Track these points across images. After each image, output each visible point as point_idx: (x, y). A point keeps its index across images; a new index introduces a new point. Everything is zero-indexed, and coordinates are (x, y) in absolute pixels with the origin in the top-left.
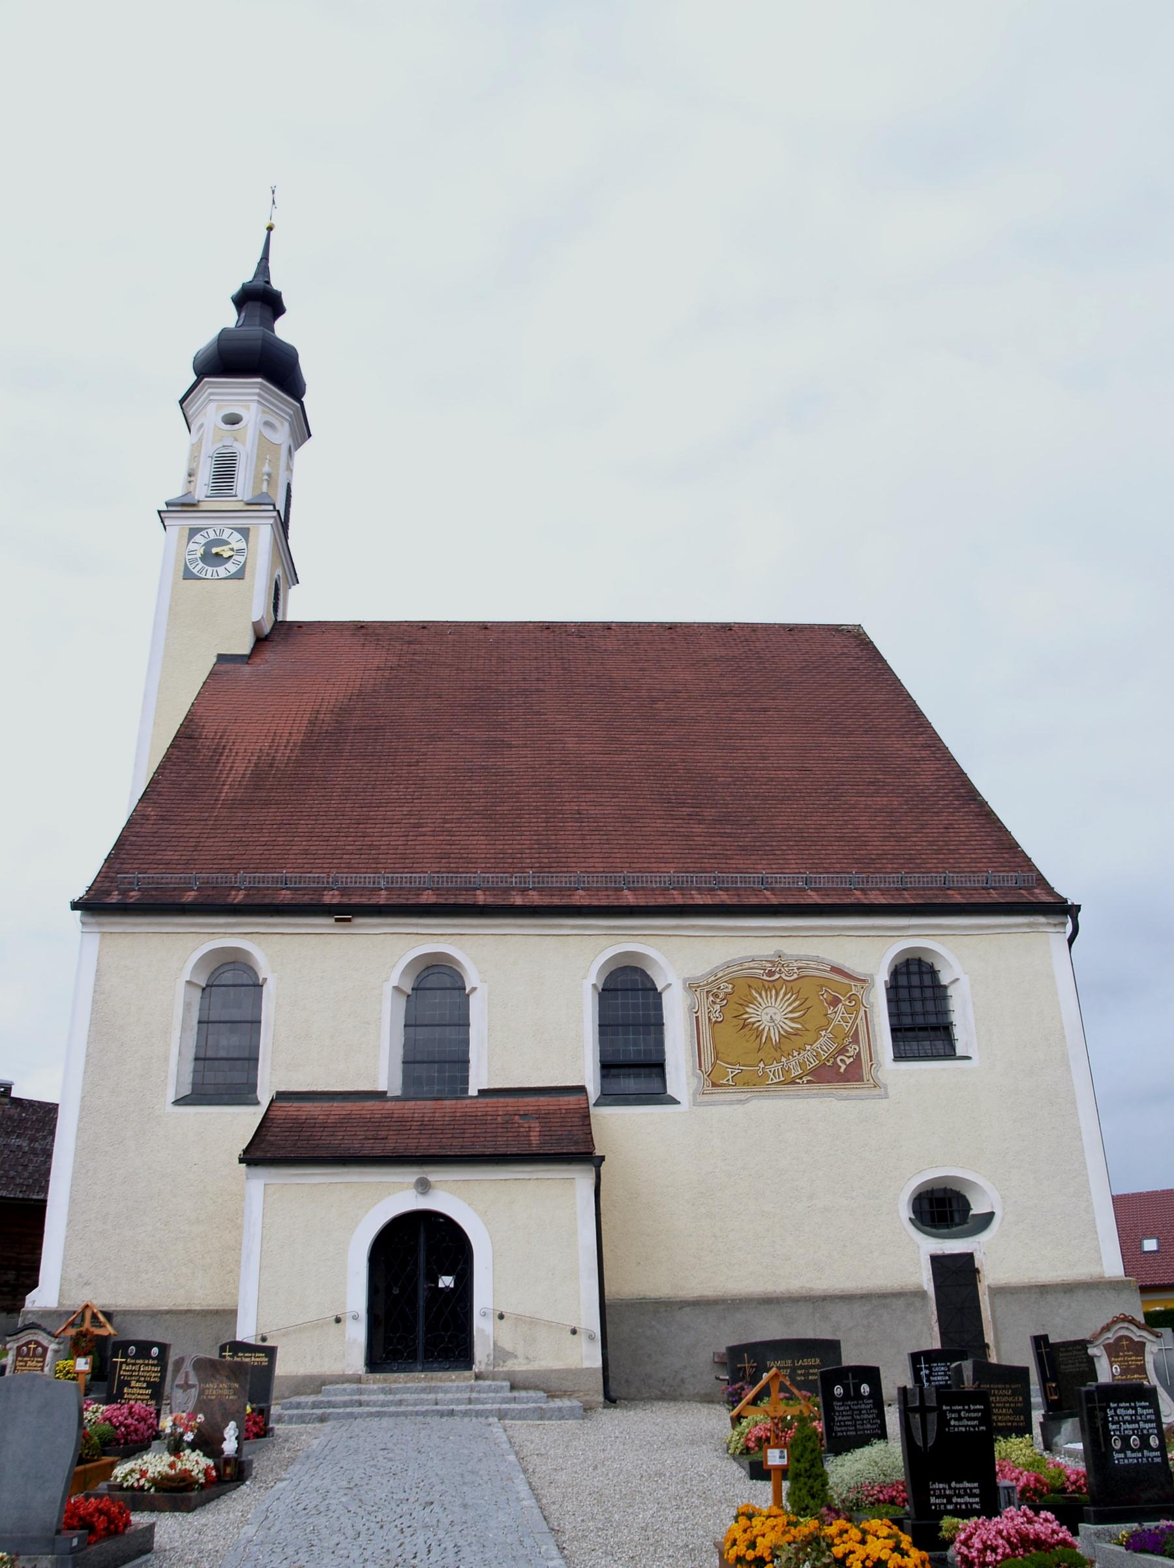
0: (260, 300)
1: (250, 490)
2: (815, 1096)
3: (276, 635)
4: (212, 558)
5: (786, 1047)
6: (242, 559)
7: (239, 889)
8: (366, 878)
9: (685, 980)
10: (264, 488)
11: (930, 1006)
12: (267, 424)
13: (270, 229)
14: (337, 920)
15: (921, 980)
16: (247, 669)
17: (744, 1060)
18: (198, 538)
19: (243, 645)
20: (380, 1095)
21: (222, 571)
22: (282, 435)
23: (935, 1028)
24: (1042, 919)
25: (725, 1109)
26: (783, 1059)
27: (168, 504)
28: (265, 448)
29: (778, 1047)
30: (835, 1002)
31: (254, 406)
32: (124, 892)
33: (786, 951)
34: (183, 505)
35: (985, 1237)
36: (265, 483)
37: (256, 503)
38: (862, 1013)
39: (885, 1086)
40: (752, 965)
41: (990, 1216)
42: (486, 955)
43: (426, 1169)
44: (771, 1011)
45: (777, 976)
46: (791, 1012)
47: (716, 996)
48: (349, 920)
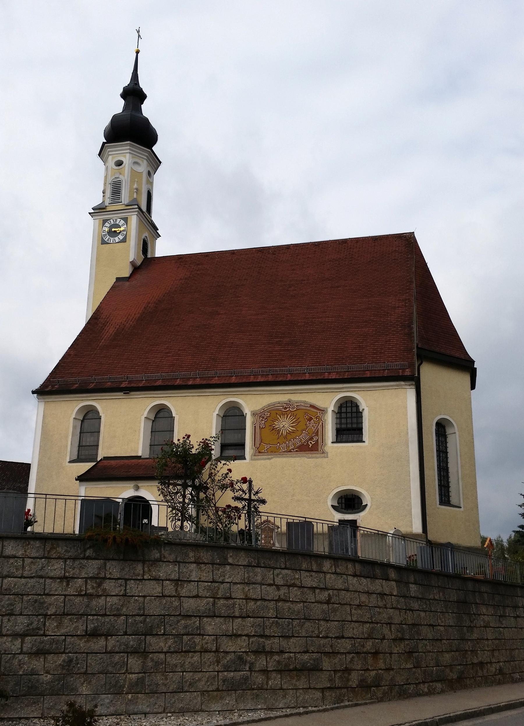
0: (134, 94)
2: (299, 457)
3: (147, 263)
4: (112, 234)
5: (289, 437)
6: (125, 233)
7: (93, 383)
8: (138, 376)
9: (252, 412)
10: (135, 196)
11: (355, 420)
12: (135, 163)
13: (138, 52)
16: (127, 284)
17: (273, 442)
18: (107, 224)
19: (126, 272)
20: (139, 457)
22: (143, 168)
23: (354, 429)
24: (402, 383)
25: (263, 461)
27: (93, 209)
28: (134, 174)
29: (285, 437)
30: (311, 419)
32: (53, 386)
34: (100, 209)
35: (362, 514)
36: (135, 194)
37: (134, 204)
39: (327, 453)
40: (278, 405)
41: (367, 505)
43: (137, 482)
48: (128, 393)
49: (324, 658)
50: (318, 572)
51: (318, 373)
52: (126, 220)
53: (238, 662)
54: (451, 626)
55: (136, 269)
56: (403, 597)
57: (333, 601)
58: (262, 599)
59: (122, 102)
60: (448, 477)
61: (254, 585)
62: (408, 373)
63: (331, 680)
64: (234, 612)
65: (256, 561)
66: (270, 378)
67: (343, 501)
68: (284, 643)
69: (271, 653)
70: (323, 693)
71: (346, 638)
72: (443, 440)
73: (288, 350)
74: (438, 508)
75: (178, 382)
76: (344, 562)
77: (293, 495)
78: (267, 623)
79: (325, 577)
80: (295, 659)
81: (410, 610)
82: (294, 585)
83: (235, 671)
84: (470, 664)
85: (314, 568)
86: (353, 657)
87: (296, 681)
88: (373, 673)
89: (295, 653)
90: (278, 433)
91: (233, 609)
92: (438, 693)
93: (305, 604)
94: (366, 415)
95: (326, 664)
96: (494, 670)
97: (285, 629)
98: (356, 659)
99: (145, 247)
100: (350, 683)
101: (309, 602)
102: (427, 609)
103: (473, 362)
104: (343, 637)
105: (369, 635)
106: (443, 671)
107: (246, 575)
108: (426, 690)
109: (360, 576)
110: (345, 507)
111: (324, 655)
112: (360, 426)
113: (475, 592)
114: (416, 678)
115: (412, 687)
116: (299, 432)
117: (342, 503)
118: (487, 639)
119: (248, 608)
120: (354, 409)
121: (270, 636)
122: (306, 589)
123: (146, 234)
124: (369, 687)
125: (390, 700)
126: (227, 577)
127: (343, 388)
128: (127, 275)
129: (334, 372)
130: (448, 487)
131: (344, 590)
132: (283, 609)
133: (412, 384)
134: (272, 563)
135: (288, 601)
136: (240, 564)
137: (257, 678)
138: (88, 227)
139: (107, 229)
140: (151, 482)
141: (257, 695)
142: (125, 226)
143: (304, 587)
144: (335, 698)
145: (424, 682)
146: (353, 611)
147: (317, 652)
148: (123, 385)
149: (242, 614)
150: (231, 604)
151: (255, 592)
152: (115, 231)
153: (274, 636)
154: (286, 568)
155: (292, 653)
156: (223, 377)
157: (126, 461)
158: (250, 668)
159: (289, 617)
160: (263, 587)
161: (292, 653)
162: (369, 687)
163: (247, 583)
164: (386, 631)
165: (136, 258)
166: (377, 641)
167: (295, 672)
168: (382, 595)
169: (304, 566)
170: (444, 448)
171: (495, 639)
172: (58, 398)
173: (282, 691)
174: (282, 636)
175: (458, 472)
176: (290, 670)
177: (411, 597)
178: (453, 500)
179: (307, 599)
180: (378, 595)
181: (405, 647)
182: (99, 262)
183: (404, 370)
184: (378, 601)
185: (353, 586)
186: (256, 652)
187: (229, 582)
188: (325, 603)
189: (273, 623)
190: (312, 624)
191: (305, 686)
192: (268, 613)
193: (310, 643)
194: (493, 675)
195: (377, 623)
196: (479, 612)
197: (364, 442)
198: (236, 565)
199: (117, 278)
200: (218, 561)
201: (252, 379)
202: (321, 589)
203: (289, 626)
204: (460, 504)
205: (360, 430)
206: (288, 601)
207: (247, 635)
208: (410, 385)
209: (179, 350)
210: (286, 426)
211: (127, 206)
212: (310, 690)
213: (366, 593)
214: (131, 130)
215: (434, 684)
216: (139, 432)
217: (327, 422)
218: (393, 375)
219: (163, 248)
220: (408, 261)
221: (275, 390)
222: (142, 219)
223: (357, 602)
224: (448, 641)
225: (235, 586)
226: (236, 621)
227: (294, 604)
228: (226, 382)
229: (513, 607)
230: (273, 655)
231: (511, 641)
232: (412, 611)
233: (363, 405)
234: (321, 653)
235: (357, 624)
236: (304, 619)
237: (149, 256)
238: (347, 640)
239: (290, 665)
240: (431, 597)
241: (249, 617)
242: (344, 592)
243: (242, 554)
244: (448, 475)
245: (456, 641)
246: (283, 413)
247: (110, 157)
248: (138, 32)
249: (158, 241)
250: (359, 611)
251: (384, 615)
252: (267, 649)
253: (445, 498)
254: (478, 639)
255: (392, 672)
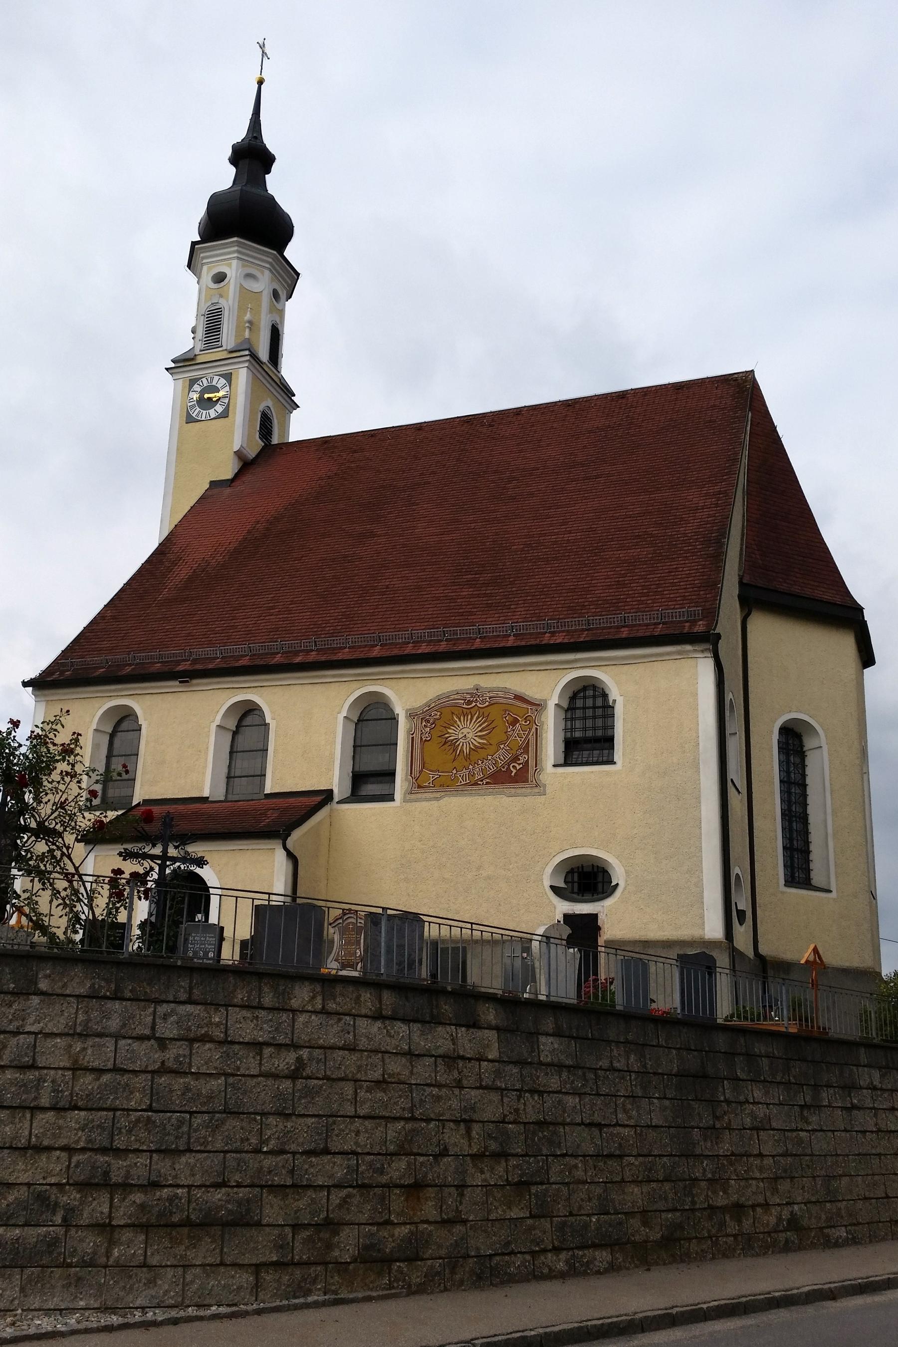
0: (252, 157)
1: (233, 338)
3: (267, 451)
4: (206, 403)
5: (474, 757)
6: (226, 401)
7: (130, 665)
8: (209, 651)
9: (407, 711)
10: (247, 334)
12: (249, 276)
13: (261, 82)
14: (180, 682)
15: (585, 703)
16: (228, 491)
18: (197, 388)
21: (212, 413)
22: (263, 284)
23: (597, 740)
24: (688, 647)
25: (424, 804)
26: (471, 767)
28: (246, 297)
29: (468, 758)
30: (515, 721)
31: (235, 263)
33: (482, 685)
35: (608, 902)
38: (534, 730)
40: (456, 697)
41: (617, 884)
42: (275, 698)
44: (465, 731)
45: (474, 704)
46: (480, 731)
47: (428, 721)
49: (268, 1197)
50: (277, 1009)
51: (531, 634)
52: (228, 377)
53: (35, 1207)
54: (656, 1126)
55: (246, 465)
56: (515, 1063)
57: (308, 1071)
58: (116, 1070)
59: (233, 170)
60: (807, 833)
61: (97, 1040)
62: (700, 627)
63: (281, 1247)
64: (36, 1098)
65: (113, 986)
66: (443, 647)
67: (576, 879)
68: (163, 1166)
69: (126, 1187)
70: (257, 1274)
71: (335, 1153)
72: (798, 760)
73: (485, 595)
74: (783, 893)
75: (278, 659)
76: (351, 989)
77: (478, 868)
78: (123, 1122)
79: (294, 1020)
80: (189, 1202)
81: (532, 1092)
82: (205, 1039)
83: (26, 1224)
84: (705, 1209)
85: (268, 999)
86: (349, 1196)
87: (187, 1248)
88: (405, 1230)
89: (189, 1187)
90: (455, 750)
91: (37, 1089)
92: (598, 1273)
93: (231, 1080)
94: (619, 711)
95: (273, 1210)
96: (773, 1220)
97: (169, 1134)
98: (356, 1200)
99: (266, 426)
100: (336, 1253)
101: (244, 1076)
102: (588, 1090)
103: (860, 610)
104: (326, 1151)
105: (401, 1147)
106: (620, 1223)
107: (81, 1017)
108: (561, 1266)
109: (393, 1018)
110: (579, 889)
111: (269, 1193)
112: (609, 733)
113: (734, 1054)
114: (532, 1241)
115: (518, 1260)
116: (494, 748)
117: (573, 882)
118: (761, 1155)
119: (76, 1089)
120: (599, 702)
121: (127, 1151)
122: (237, 1047)
123: (269, 403)
124: (388, 1261)
125: (446, 1290)
126: (31, 1020)
127: (576, 661)
128: (229, 475)
129: (563, 632)
130: (808, 852)
131: (340, 1048)
132: (171, 1091)
133: (706, 650)
134: (154, 991)
135: (185, 1073)
136: (68, 992)
137: (81, 1240)
138: (162, 396)
139: (195, 396)
140: (214, 843)
141: (79, 1279)
142: (227, 388)
143: (232, 1043)
144: (288, 1286)
145: (556, 1250)
146: (362, 1094)
147: (251, 1186)
148: (180, 668)
149: (57, 1103)
150: (31, 1081)
151: (98, 1054)
152: (210, 399)
153: (137, 1151)
154: (190, 1001)
155: (183, 1186)
156: (360, 647)
157: (180, 807)
158: (65, 1219)
159: (183, 1109)
160: (122, 1043)
161: (183, 1186)
162: (388, 1261)
163: (80, 1035)
164: (454, 1137)
165: (245, 446)
166: (421, 1159)
167: (185, 1230)
168: (451, 1059)
169: (240, 996)
170: (799, 777)
171: (784, 1155)
172: (67, 694)
173: (145, 1269)
174: (158, 1151)
175: (825, 821)
176: (174, 1226)
177: (541, 1063)
178: (817, 878)
179: (238, 1069)
180: (440, 1060)
181: (507, 1172)
182: (182, 453)
183: (694, 622)
184: (436, 1072)
185: (370, 1040)
186: (85, 1186)
187: (34, 1033)
188: (286, 1077)
189: (138, 1121)
190: (244, 1124)
191: (209, 1260)
192: (129, 1100)
193: (235, 1164)
194: (769, 1233)
195: (428, 1120)
196: (742, 1098)
197: (615, 763)
198: (58, 995)
199: (211, 482)
200: (12, 986)
201: (409, 650)
202: (279, 1046)
203: (179, 1127)
204: (829, 883)
205: (608, 741)
206: (185, 1073)
207: (63, 1149)
208: (702, 651)
209: (292, 602)
210: (470, 736)
211: (231, 352)
212: (222, 1269)
213: (404, 1054)
214: (248, 216)
215: (589, 1253)
216: (206, 753)
217: (545, 727)
218: (672, 632)
219: (301, 427)
220: (735, 423)
221: (453, 669)
222: (255, 371)
223: (377, 1075)
224: (641, 1159)
225: (49, 1040)
226: (41, 1116)
227: (202, 1081)
228: (362, 656)
229: (843, 1088)
230: (130, 1193)
231: (829, 1159)
232: (541, 1093)
233: (615, 694)
234: (262, 1187)
235: (368, 1124)
236: (224, 1112)
237: (275, 440)
238: (338, 1159)
239: (171, 1213)
240: (604, 1063)
241: (76, 1108)
242: (341, 1053)
243: (78, 970)
244: (807, 829)
245: (665, 1159)
246: (465, 710)
247: (205, 268)
248: (262, 47)
249: (295, 415)
250: (380, 1095)
251: (455, 1103)
252: (116, 1177)
253: (799, 872)
254: (733, 1154)
255: (459, 1229)
